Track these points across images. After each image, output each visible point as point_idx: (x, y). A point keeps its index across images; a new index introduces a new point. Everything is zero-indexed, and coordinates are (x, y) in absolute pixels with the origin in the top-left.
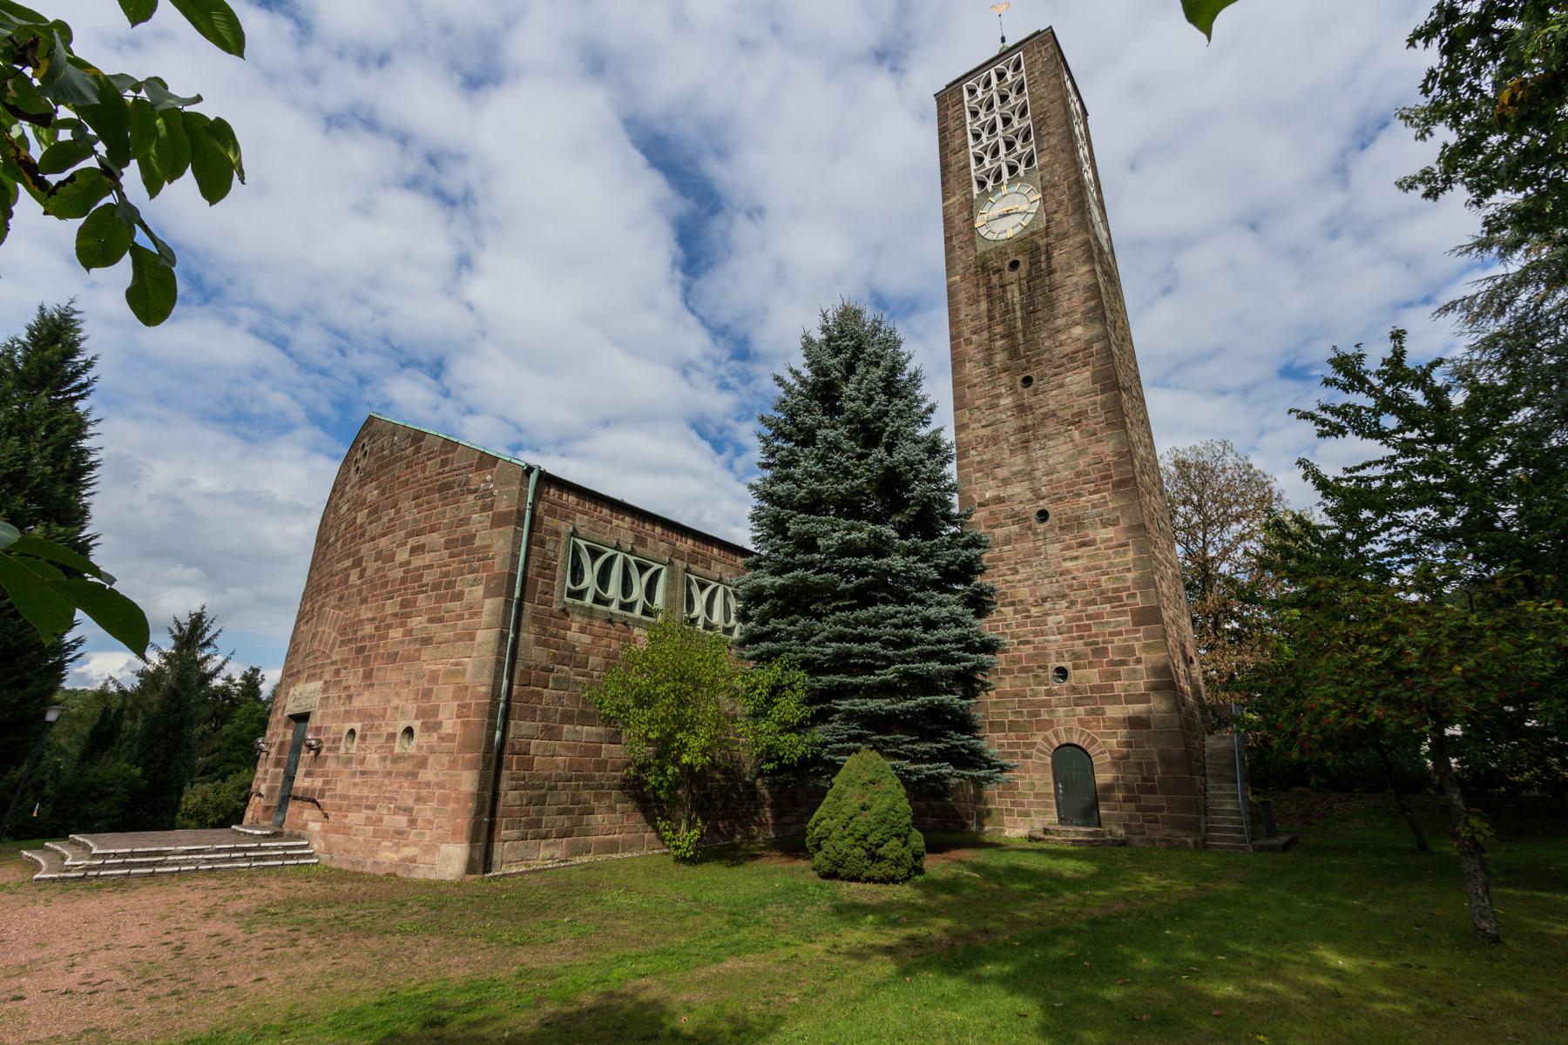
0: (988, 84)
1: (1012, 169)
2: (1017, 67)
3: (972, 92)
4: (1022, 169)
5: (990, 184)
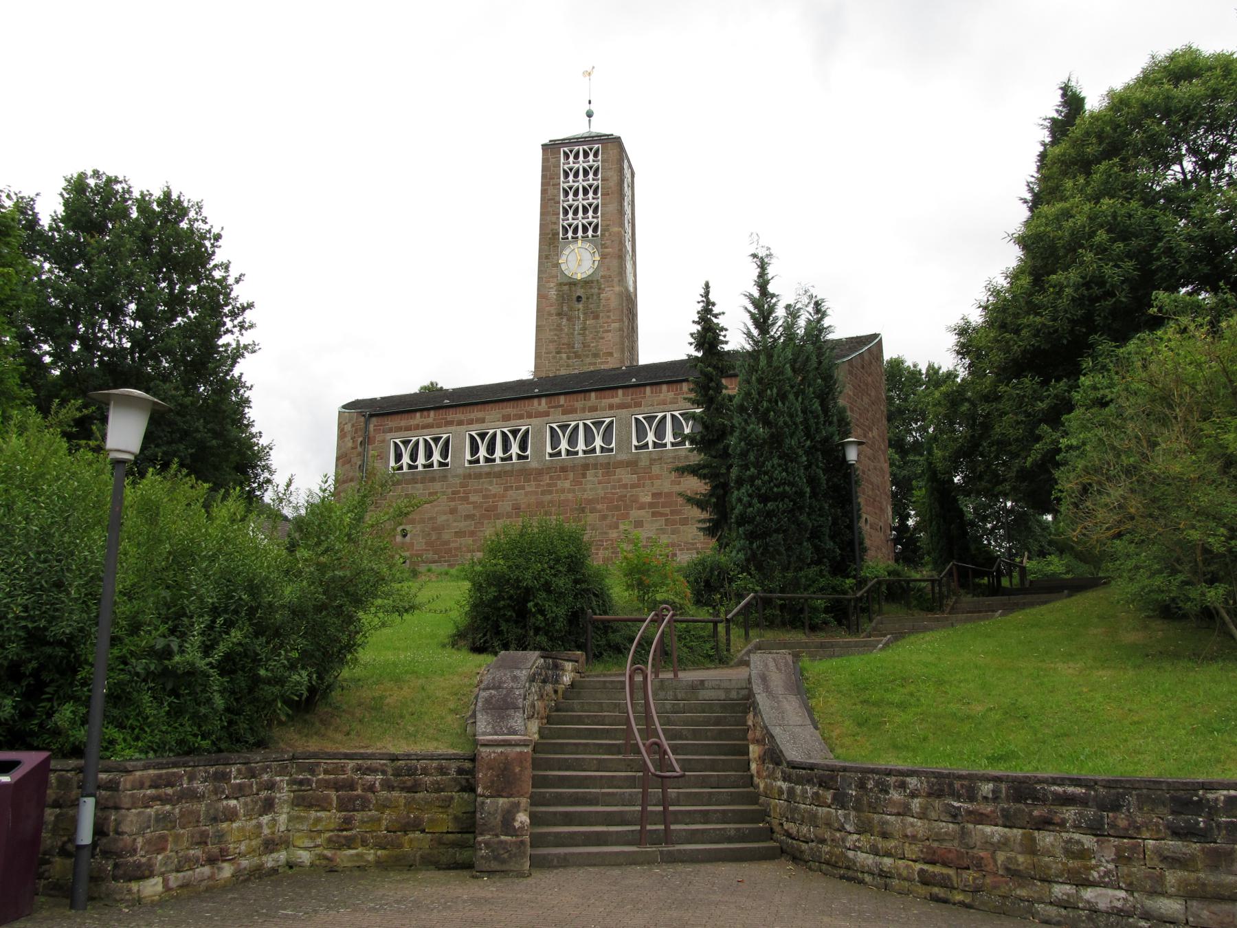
0: (576, 156)
1: (585, 229)
2: (596, 155)
3: (567, 156)
4: (590, 233)
5: (570, 234)
